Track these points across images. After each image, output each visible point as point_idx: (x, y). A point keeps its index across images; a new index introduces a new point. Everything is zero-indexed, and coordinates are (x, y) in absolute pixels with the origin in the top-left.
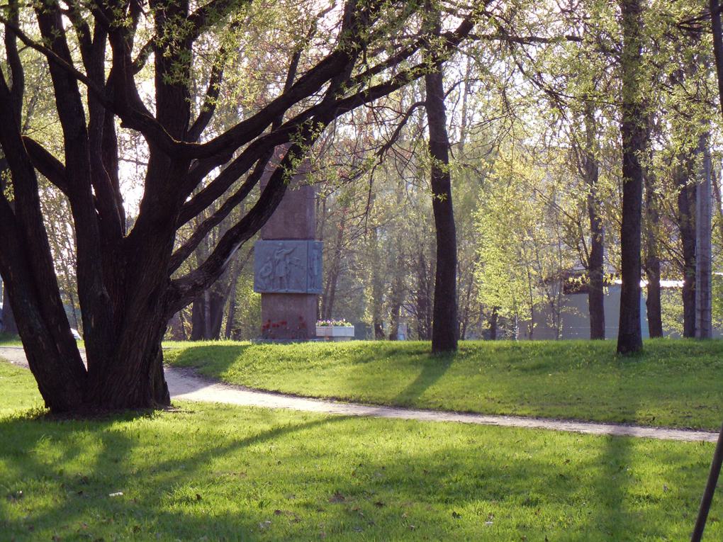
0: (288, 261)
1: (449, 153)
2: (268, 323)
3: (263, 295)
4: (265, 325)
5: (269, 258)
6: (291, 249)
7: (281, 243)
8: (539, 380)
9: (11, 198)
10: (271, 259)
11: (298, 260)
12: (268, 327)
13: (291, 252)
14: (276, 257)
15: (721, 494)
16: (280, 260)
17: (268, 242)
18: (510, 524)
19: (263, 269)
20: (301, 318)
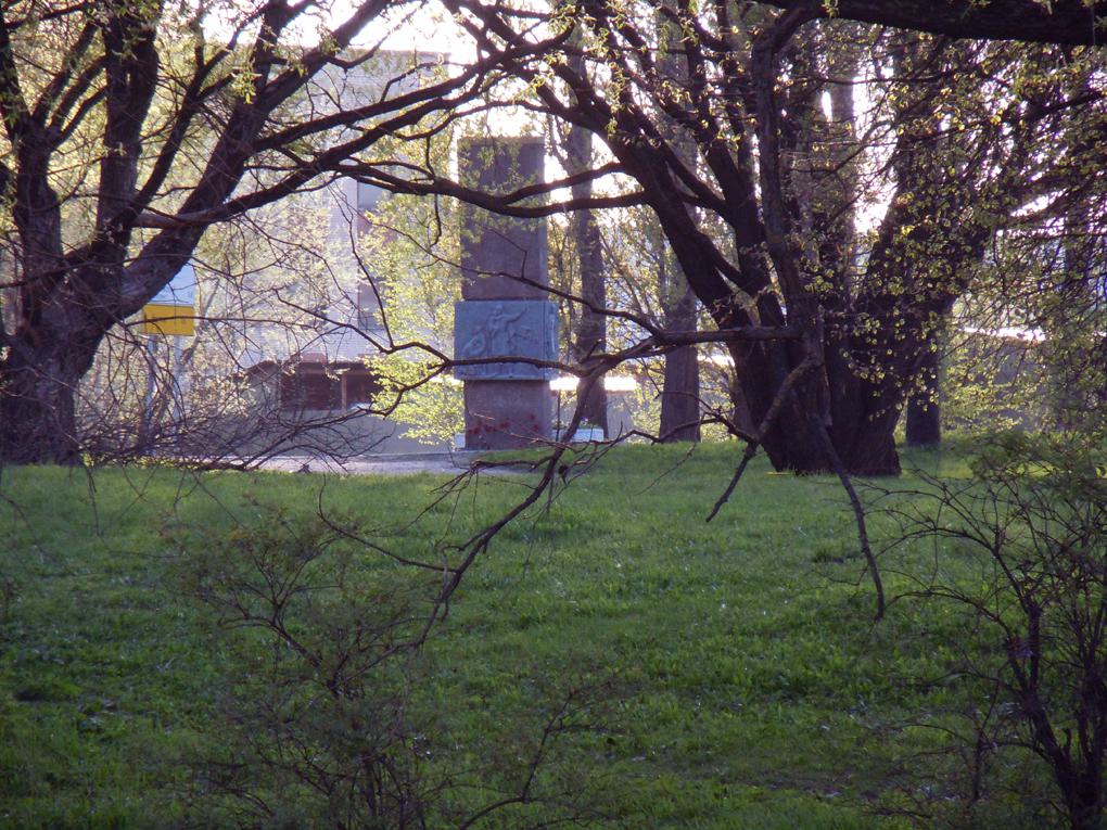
0: (512, 333)
1: (180, 107)
2: (476, 426)
3: (468, 383)
4: (472, 428)
5: (479, 328)
6: (518, 315)
7: (499, 305)
8: (63, 581)
9: (134, 251)
10: (483, 329)
11: (528, 331)
12: (477, 431)
13: (518, 318)
14: (491, 326)
15: (1056, 810)
16: (499, 331)
17: (478, 303)
18: (706, 805)
19: (469, 344)
20: (533, 417)
